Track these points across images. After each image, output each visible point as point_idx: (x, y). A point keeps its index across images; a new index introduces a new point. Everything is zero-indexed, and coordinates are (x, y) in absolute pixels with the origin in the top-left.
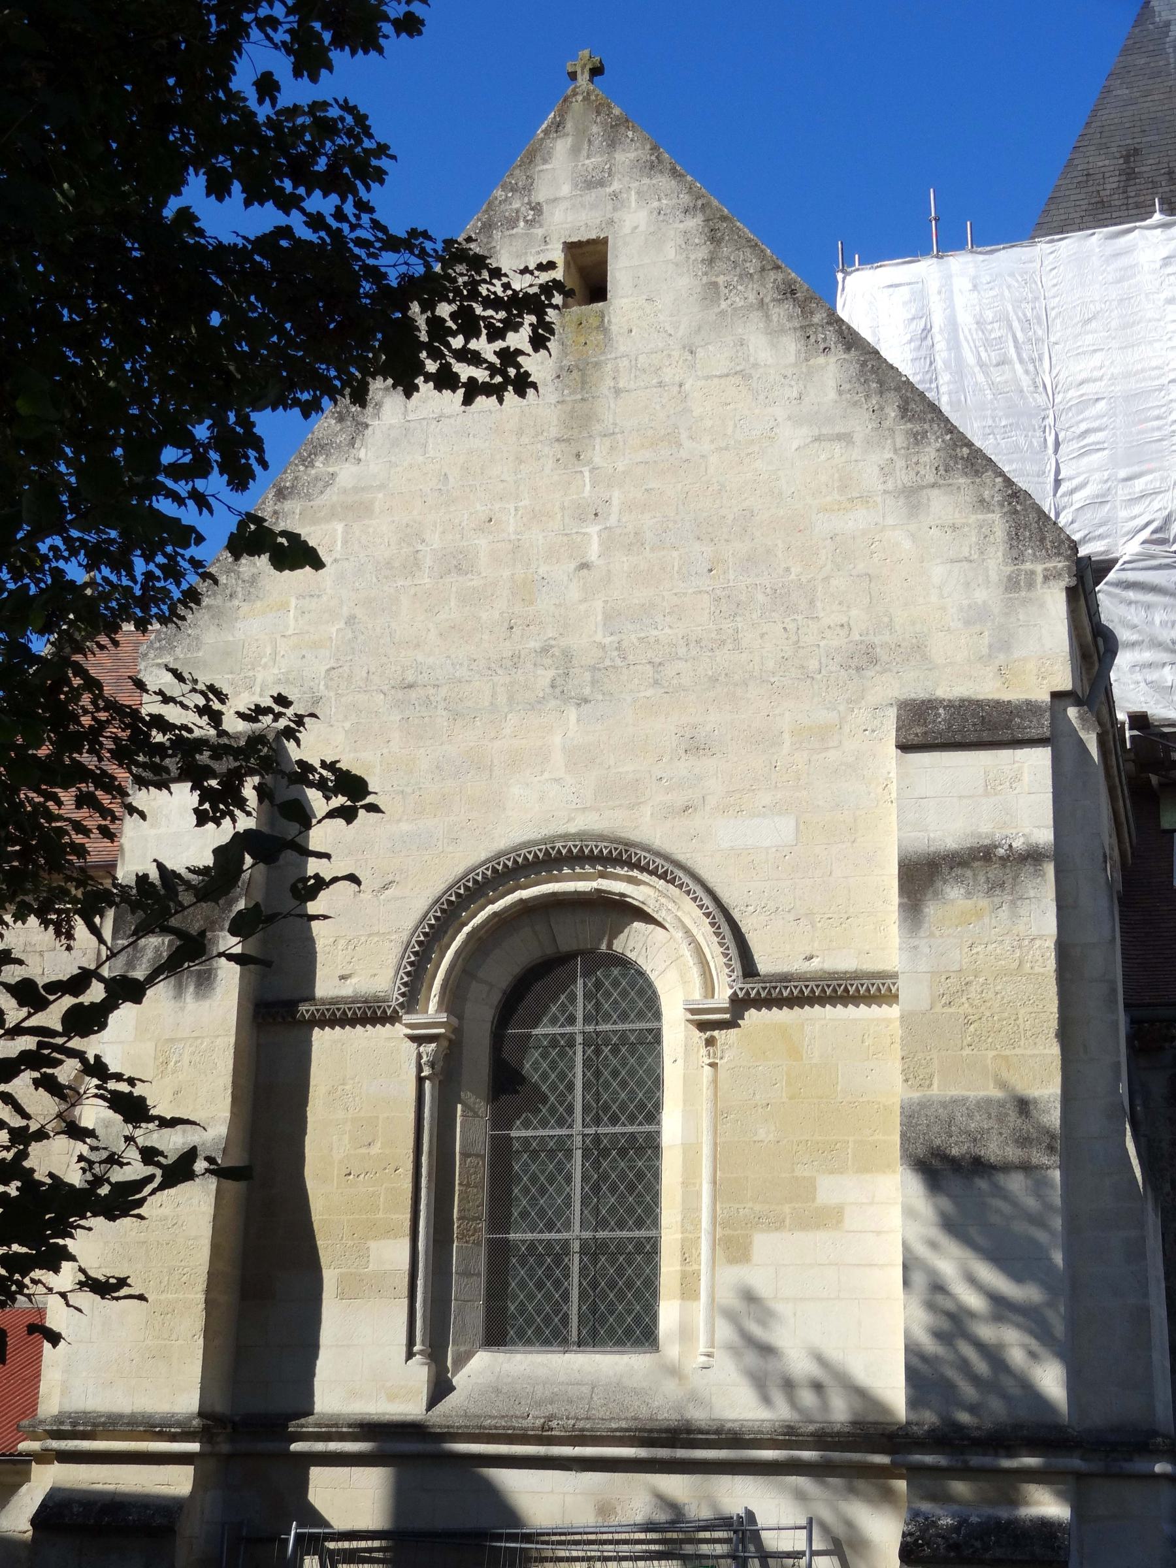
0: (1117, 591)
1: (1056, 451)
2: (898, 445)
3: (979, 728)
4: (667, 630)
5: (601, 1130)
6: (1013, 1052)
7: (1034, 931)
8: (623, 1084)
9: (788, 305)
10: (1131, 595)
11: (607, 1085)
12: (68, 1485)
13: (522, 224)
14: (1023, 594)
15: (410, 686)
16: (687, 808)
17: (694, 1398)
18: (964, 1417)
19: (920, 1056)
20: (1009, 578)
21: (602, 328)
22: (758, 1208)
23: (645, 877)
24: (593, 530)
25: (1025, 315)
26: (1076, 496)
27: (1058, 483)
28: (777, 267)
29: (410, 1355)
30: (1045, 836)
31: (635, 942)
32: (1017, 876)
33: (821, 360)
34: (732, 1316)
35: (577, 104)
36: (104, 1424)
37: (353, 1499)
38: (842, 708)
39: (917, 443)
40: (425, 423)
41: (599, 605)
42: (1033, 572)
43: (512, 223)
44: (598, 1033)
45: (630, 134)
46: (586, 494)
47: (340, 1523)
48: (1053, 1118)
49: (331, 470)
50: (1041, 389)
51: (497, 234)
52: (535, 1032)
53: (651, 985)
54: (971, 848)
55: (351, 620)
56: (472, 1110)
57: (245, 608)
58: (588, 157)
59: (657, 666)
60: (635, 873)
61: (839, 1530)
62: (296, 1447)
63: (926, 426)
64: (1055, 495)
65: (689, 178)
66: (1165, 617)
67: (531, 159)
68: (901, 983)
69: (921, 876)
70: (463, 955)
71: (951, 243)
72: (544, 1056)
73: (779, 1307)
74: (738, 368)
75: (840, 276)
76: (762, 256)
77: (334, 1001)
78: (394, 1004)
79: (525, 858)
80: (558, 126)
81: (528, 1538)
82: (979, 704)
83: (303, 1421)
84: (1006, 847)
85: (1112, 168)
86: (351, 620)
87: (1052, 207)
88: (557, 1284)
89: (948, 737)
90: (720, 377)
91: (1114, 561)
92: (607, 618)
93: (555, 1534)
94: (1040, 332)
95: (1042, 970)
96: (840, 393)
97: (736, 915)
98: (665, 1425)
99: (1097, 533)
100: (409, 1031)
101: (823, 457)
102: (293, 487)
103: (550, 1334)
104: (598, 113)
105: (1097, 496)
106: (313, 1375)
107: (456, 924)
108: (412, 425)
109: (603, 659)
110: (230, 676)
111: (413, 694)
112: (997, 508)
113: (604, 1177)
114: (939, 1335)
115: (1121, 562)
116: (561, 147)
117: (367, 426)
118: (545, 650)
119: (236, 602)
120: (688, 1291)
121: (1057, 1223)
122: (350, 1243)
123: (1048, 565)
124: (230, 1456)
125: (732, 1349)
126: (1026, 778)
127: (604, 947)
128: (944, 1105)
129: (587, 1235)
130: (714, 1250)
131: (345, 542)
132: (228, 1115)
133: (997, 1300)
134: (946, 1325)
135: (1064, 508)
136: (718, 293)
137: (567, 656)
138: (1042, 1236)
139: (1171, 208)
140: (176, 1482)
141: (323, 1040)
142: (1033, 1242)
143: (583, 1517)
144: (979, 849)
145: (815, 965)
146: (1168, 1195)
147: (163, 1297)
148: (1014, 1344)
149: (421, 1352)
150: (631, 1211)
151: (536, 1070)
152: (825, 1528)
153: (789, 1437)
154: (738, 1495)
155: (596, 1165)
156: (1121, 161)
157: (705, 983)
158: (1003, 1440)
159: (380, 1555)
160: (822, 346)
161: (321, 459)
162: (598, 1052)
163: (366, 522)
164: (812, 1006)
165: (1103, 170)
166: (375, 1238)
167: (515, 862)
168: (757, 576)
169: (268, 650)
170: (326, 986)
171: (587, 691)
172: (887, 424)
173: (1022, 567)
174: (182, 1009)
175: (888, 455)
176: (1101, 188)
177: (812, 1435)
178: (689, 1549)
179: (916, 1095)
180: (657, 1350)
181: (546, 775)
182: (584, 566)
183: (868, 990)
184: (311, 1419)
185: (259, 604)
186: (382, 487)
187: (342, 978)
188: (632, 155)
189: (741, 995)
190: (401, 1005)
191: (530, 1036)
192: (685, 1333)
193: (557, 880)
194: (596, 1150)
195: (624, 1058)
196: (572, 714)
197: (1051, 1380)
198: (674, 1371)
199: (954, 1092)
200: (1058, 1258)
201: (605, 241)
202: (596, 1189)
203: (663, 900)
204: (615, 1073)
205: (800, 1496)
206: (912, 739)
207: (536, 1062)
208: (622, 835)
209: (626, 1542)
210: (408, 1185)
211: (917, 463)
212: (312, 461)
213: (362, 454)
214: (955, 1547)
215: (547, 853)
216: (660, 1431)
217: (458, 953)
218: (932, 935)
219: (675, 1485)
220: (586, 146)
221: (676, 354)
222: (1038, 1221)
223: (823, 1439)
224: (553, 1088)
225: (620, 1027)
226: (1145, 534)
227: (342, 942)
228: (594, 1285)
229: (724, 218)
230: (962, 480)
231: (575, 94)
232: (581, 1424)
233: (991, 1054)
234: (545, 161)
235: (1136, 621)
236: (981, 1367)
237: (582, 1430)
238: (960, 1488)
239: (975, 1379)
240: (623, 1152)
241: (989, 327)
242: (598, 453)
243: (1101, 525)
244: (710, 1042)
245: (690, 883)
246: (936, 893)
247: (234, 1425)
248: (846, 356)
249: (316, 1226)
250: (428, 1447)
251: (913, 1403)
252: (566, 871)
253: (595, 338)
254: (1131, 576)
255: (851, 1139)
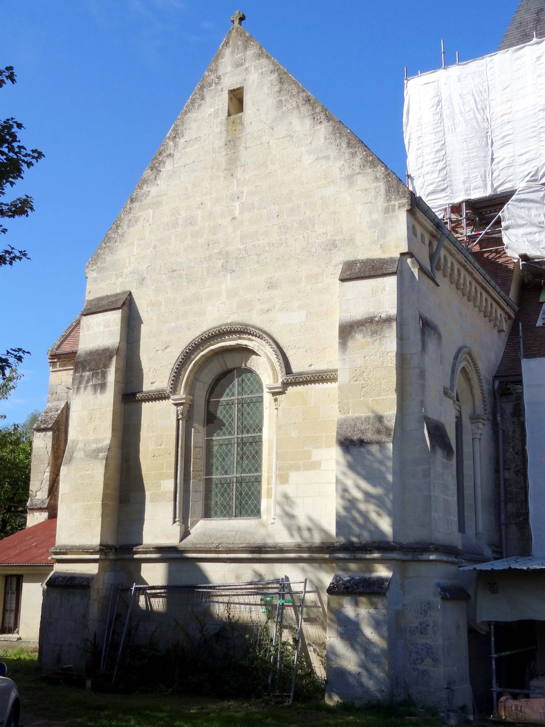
0: (516, 203)
1: (492, 147)
2: (346, 158)
3: (371, 270)
4: (262, 241)
5: (244, 436)
6: (379, 398)
7: (388, 350)
8: (251, 418)
9: (307, 106)
10: (522, 204)
11: (246, 419)
12: (60, 571)
13: (214, 85)
14: (391, 214)
15: (174, 271)
16: (269, 310)
17: (270, 536)
18: (354, 539)
19: (345, 401)
20: (386, 208)
21: (241, 123)
22: (291, 463)
23: (253, 338)
24: (237, 204)
25: (479, 90)
26: (499, 165)
27: (493, 159)
28: (304, 91)
29: (174, 522)
30: (393, 311)
31: (254, 363)
32: (382, 328)
33: (319, 127)
34: (279, 504)
35: (234, 34)
36: (69, 549)
37: (154, 574)
38: (323, 266)
39: (353, 157)
40: (180, 168)
41: (239, 233)
42: (394, 205)
43: (210, 85)
44: (242, 399)
45: (252, 43)
46: (235, 190)
47: (151, 584)
48: (391, 423)
49: (148, 190)
50: (486, 120)
51: (205, 90)
52: (221, 400)
53: (260, 380)
54: (366, 318)
55: (155, 247)
56: (197, 430)
57: (120, 245)
58: (237, 55)
59: (258, 255)
60: (250, 337)
61: (317, 583)
62: (136, 556)
63: (357, 150)
64: (491, 165)
65: (273, 58)
66: (536, 213)
67: (217, 58)
68: (339, 373)
69: (347, 331)
70: (193, 372)
71: (450, 62)
72: (224, 409)
73: (294, 499)
74: (289, 134)
75: (405, 81)
76: (298, 87)
77: (148, 392)
78: (168, 392)
79: (212, 334)
80: (227, 43)
81: (214, 587)
82: (373, 260)
83: (138, 547)
84: (379, 317)
85: (531, 19)
86: (155, 247)
87: (505, 39)
88: (229, 494)
89: (359, 275)
90: (282, 138)
91: (515, 191)
92: (242, 238)
93: (222, 586)
94: (485, 96)
95: (391, 365)
96: (325, 139)
97: (285, 351)
98: (257, 545)
99: (509, 179)
100: (173, 402)
101: (319, 166)
102: (136, 197)
103: (226, 512)
104: (241, 36)
105: (509, 164)
106: (142, 530)
107: (190, 360)
108: (176, 169)
109: (239, 254)
110: (115, 272)
111: (175, 273)
112: (382, 181)
113: (244, 454)
114: (345, 508)
115: (518, 191)
116: (228, 52)
117: (161, 171)
118: (220, 253)
119: (117, 244)
120: (269, 496)
121: (390, 464)
122: (155, 481)
123: (400, 202)
124: (115, 560)
125: (281, 517)
126: (387, 289)
127: (243, 366)
128: (353, 420)
129: (238, 475)
130: (276, 479)
131: (153, 217)
132: (111, 436)
133: (367, 495)
134: (348, 504)
135: (495, 170)
136: (282, 104)
137: (228, 254)
138: (383, 469)
139: (540, 35)
140: (92, 569)
141: (146, 406)
142: (380, 471)
143: (231, 580)
144: (368, 319)
145: (313, 368)
146: (511, 453)
147: (88, 503)
148: (372, 511)
149: (178, 521)
150: (253, 465)
151: (221, 414)
152: (311, 582)
153: (299, 549)
154: (283, 571)
155: (242, 449)
156: (535, 15)
157: (274, 377)
158: (366, 548)
159: (164, 595)
160: (319, 121)
161: (145, 185)
162: (242, 406)
163: (160, 209)
164: (323, 383)
165: (527, 20)
166: (163, 479)
167: (209, 335)
168: (294, 216)
169: (128, 261)
170: (147, 387)
171: (234, 267)
172: (342, 150)
173: (391, 203)
174: (96, 398)
175: (342, 163)
176: (525, 28)
177: (307, 548)
178: (265, 591)
179: (343, 416)
180: (261, 517)
181: (220, 301)
182: (234, 218)
183: (330, 377)
184: (141, 546)
185: (125, 244)
186: (165, 194)
187: (152, 383)
188: (253, 52)
189: (285, 381)
190: (171, 392)
191: (219, 401)
192: (268, 510)
193: (218, 343)
194: (242, 443)
195: (252, 408)
196: (229, 276)
197: (385, 525)
198: (264, 525)
199: (357, 415)
200: (390, 478)
201: (243, 87)
202: (242, 458)
203: (261, 346)
204: (248, 414)
205: (303, 570)
206: (346, 277)
207: (221, 411)
208: (246, 322)
209: (245, 589)
210: (173, 459)
211: (353, 165)
212: (142, 187)
213: (159, 183)
214: (347, 588)
215: (219, 331)
216: (256, 547)
217: (191, 372)
218: (350, 354)
219: (260, 567)
220: (236, 50)
221: (267, 130)
222: (381, 463)
223: (311, 549)
224: (227, 421)
225: (250, 396)
226: (528, 178)
227: (152, 370)
228: (241, 494)
229: (285, 73)
230: (369, 170)
231: (233, 29)
232: (229, 546)
233: (371, 399)
234: (222, 58)
235: (524, 215)
236: (361, 520)
237: (229, 548)
238: (353, 566)
239: (359, 525)
240: (251, 443)
241: (464, 97)
242: (239, 174)
243: (509, 176)
244: (276, 400)
245: (268, 339)
246: (352, 337)
247: (116, 549)
248: (328, 124)
249: (143, 476)
250: (179, 555)
251: (337, 534)
252: (227, 337)
253: (239, 127)
254: (522, 197)
255: (324, 435)
